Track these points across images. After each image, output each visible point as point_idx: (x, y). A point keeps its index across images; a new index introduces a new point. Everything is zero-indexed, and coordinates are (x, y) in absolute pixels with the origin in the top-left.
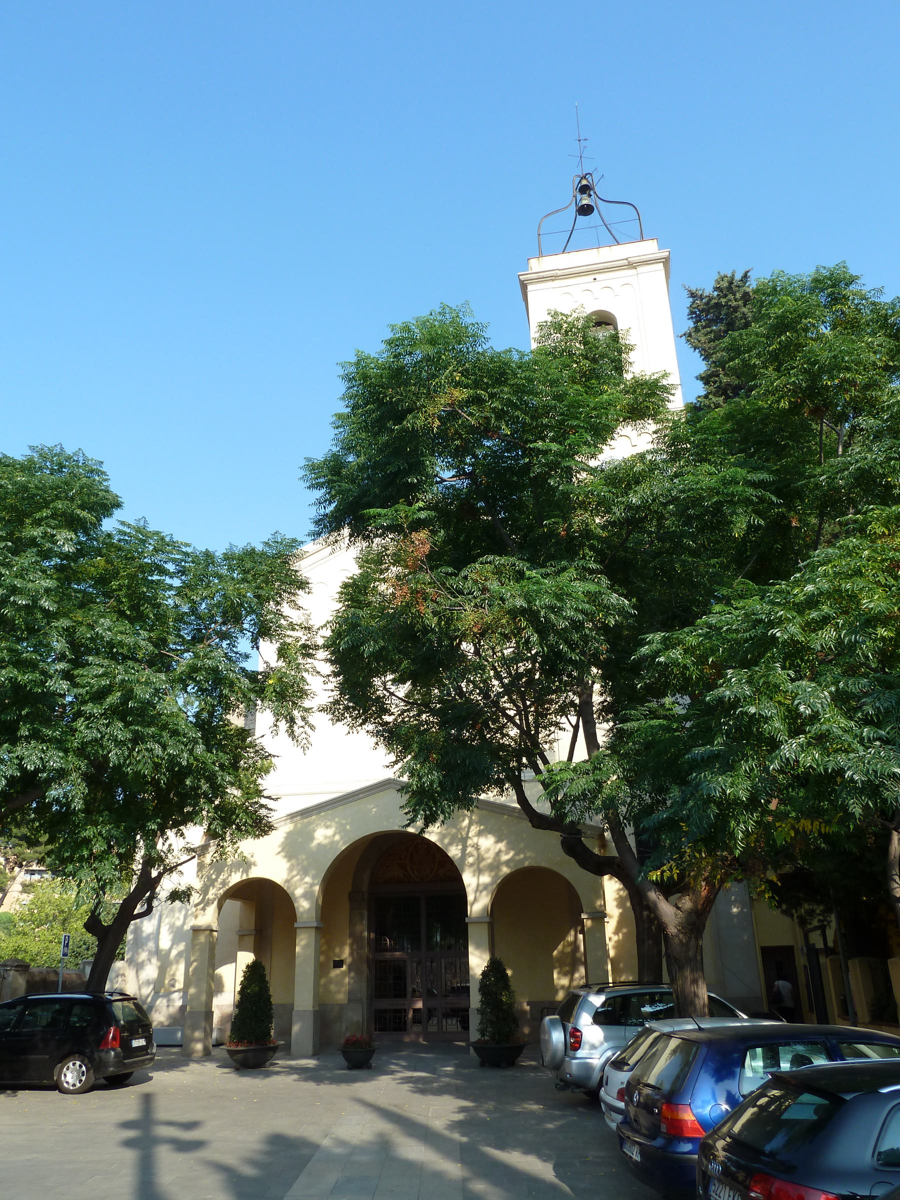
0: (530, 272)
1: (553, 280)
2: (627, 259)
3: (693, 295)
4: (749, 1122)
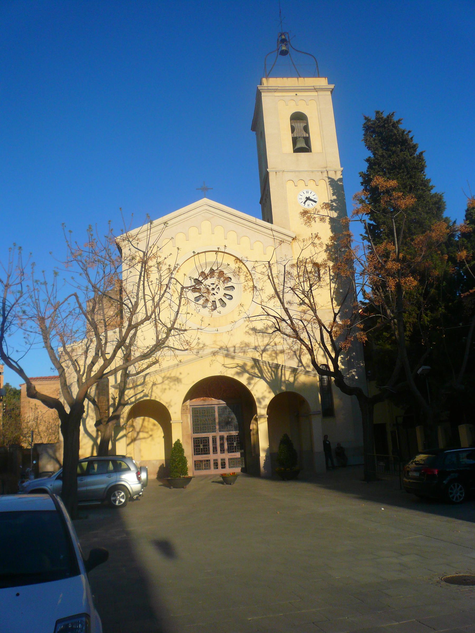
0: (262, 86)
1: (275, 92)
2: (313, 86)
3: (366, 118)
4: (469, 271)
